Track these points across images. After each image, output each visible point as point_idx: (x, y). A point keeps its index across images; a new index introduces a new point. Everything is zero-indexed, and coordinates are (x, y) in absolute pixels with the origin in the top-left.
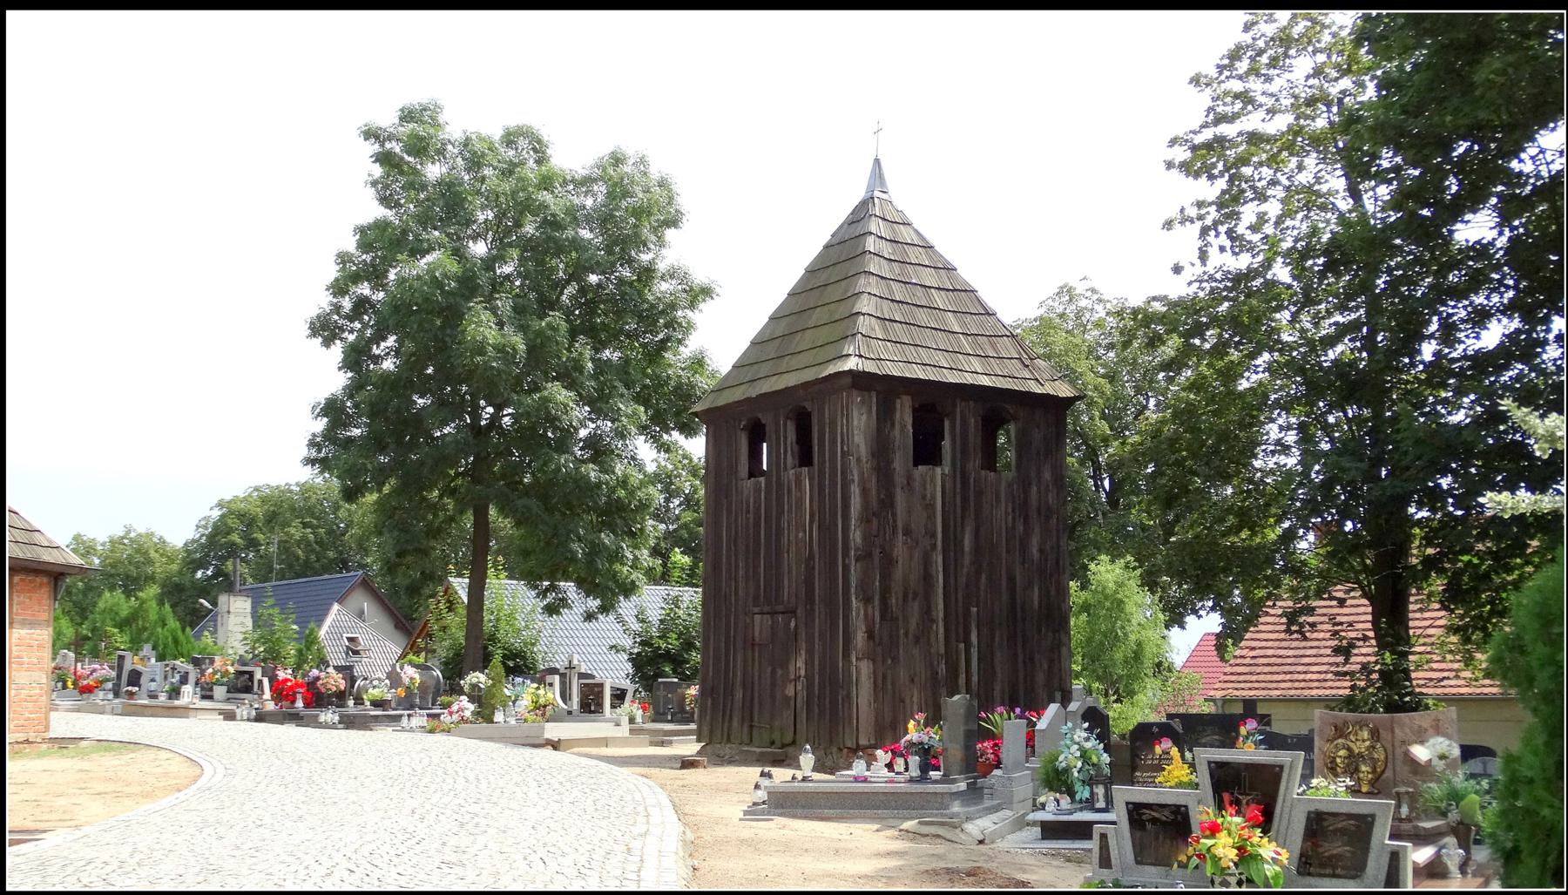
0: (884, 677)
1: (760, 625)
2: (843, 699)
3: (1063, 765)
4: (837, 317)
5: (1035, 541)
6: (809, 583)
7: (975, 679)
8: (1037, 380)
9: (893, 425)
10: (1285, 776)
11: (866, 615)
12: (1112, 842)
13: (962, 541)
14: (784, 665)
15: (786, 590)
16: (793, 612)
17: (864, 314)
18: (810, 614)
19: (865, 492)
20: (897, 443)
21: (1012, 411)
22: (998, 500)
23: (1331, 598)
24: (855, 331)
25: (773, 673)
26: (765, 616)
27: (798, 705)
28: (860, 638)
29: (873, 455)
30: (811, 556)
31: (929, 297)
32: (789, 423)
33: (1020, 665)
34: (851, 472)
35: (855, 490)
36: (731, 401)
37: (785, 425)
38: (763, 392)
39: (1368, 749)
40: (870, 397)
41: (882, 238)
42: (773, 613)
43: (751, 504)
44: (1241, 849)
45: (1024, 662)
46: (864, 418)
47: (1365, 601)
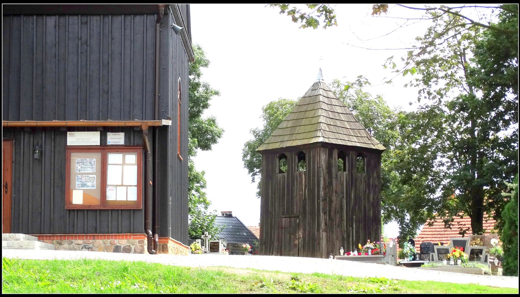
0: (329, 238)
1: (285, 221)
2: (317, 244)
3: (406, 252)
4: (313, 123)
5: (371, 196)
6: (304, 208)
7: (354, 239)
8: (373, 144)
9: (332, 159)
10: (467, 242)
11: (325, 218)
12: (434, 256)
13: (351, 195)
14: (294, 234)
15: (295, 210)
16: (298, 217)
17: (322, 123)
18: (305, 217)
19: (324, 179)
20: (333, 164)
21: (366, 154)
22: (361, 182)
23: (459, 216)
24: (320, 128)
25: (290, 237)
26: (287, 219)
27: (300, 247)
28: (323, 225)
29: (327, 169)
30: (305, 199)
31: (339, 116)
32: (296, 156)
33: (367, 235)
34: (321, 173)
35: (322, 179)
36: (275, 148)
37: (295, 157)
38: (288, 146)
39: (479, 243)
40: (326, 150)
41: (324, 96)
42: (290, 217)
43: (281, 182)
44: (460, 254)
45: (368, 234)
46: (324, 156)
47: (468, 217)
